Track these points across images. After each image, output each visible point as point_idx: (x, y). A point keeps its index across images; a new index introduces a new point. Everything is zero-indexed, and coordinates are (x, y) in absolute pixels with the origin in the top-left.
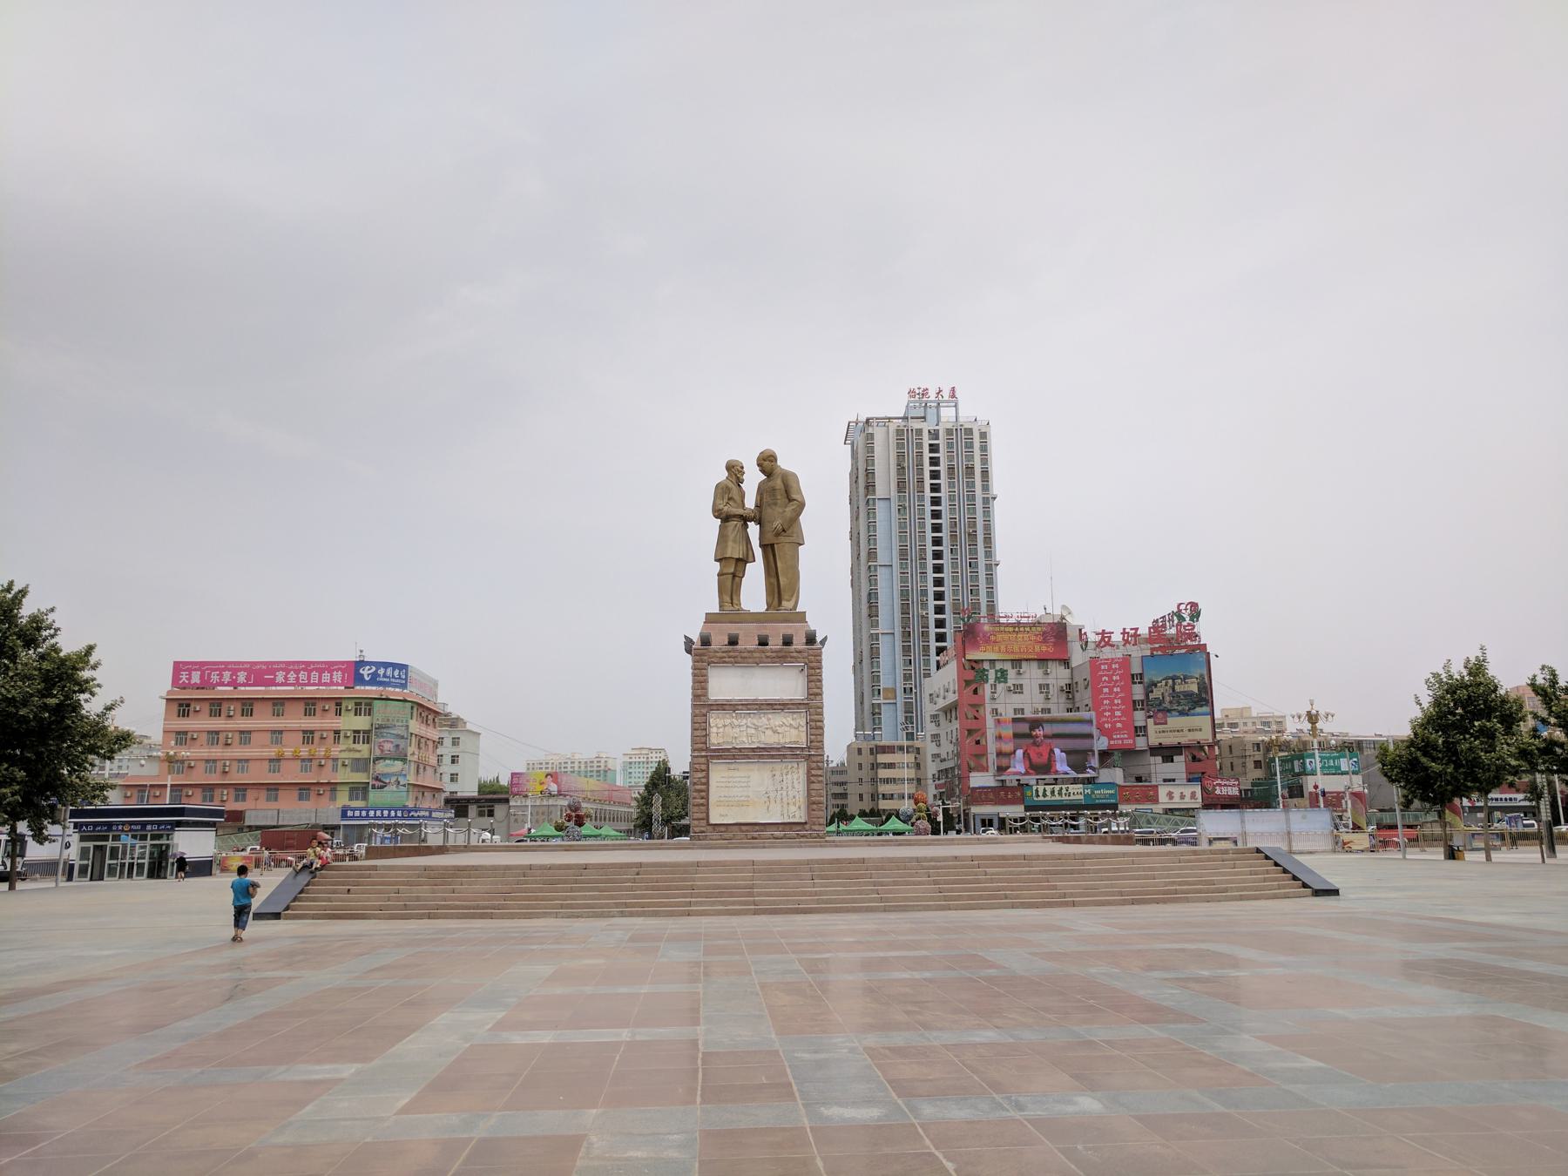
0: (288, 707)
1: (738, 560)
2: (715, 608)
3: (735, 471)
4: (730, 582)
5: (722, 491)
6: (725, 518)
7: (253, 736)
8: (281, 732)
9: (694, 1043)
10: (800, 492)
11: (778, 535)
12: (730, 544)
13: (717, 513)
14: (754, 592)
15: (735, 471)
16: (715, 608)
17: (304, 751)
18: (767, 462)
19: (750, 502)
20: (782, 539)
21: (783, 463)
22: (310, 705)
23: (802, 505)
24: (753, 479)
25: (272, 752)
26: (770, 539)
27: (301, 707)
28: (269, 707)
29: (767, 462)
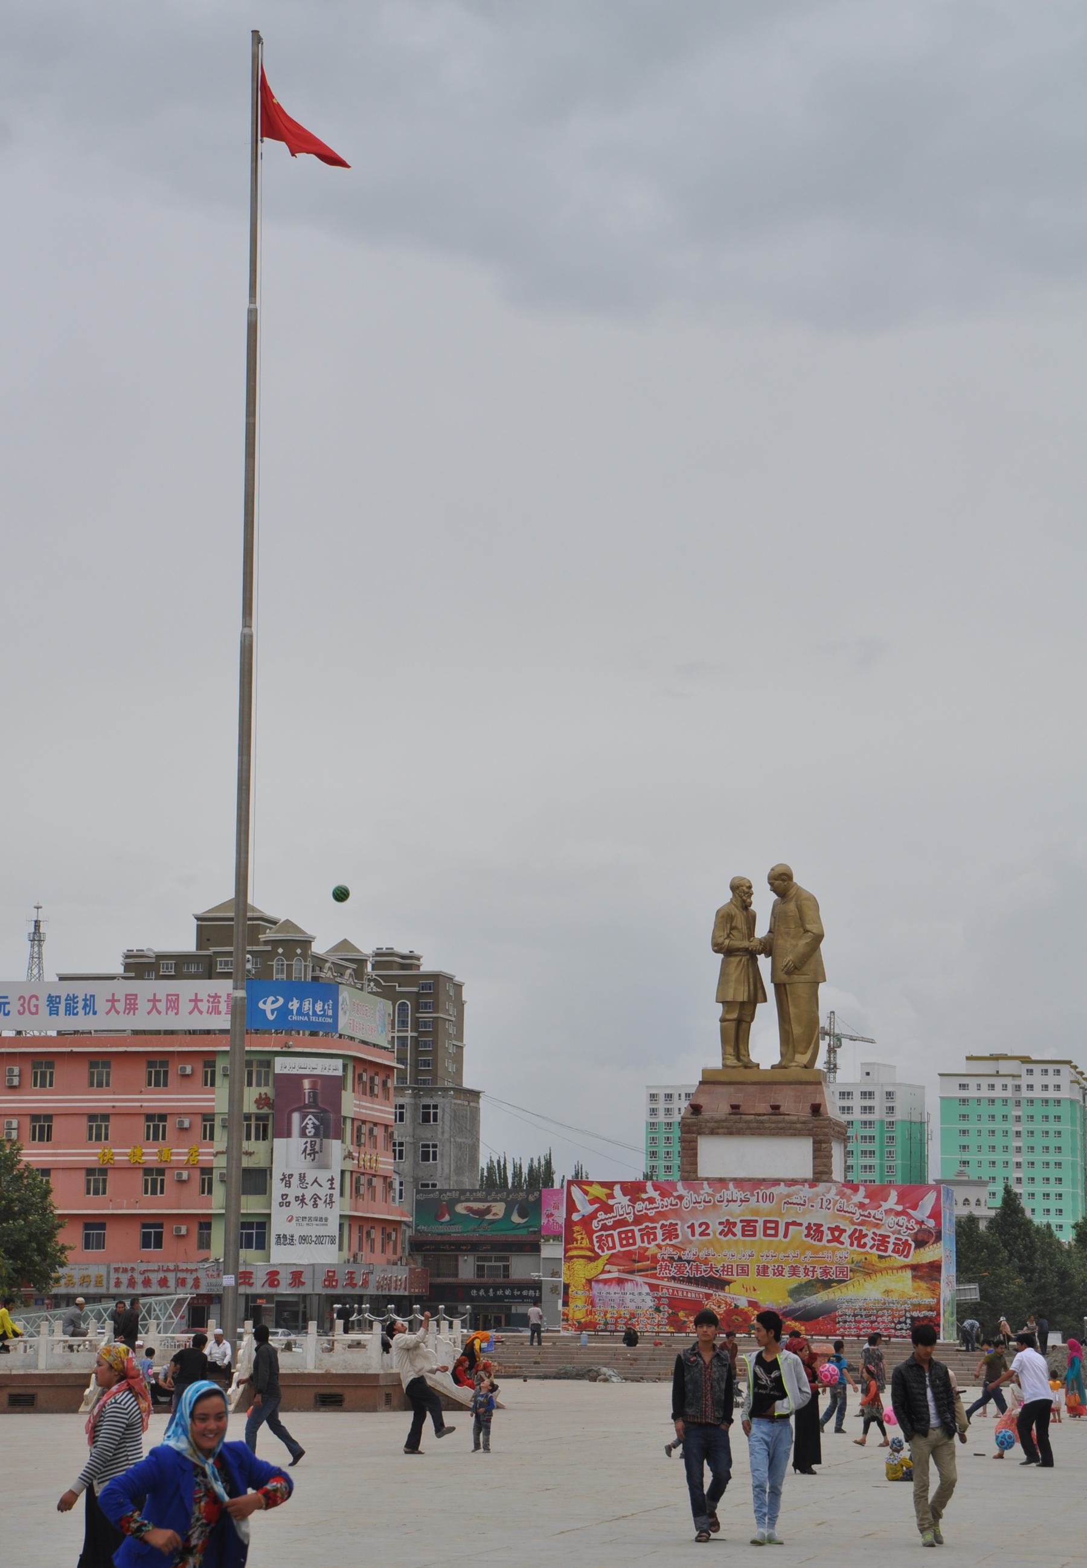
0: (117, 1072)
1: (742, 1003)
2: (715, 1061)
3: (741, 891)
4: (736, 1031)
5: (725, 919)
6: (729, 952)
7: (113, 1122)
8: (106, 1117)
9: (395, 1088)
10: (818, 920)
11: (789, 973)
12: (732, 984)
13: (718, 948)
14: (765, 1045)
15: (741, 891)
16: (715, 1061)
17: (150, 1155)
18: (781, 881)
19: (762, 930)
20: (796, 978)
21: (800, 879)
22: (158, 1067)
23: (819, 937)
24: (763, 902)
25: (91, 1155)
26: (783, 977)
27: (141, 1071)
28: (82, 1071)
29: (781, 881)
